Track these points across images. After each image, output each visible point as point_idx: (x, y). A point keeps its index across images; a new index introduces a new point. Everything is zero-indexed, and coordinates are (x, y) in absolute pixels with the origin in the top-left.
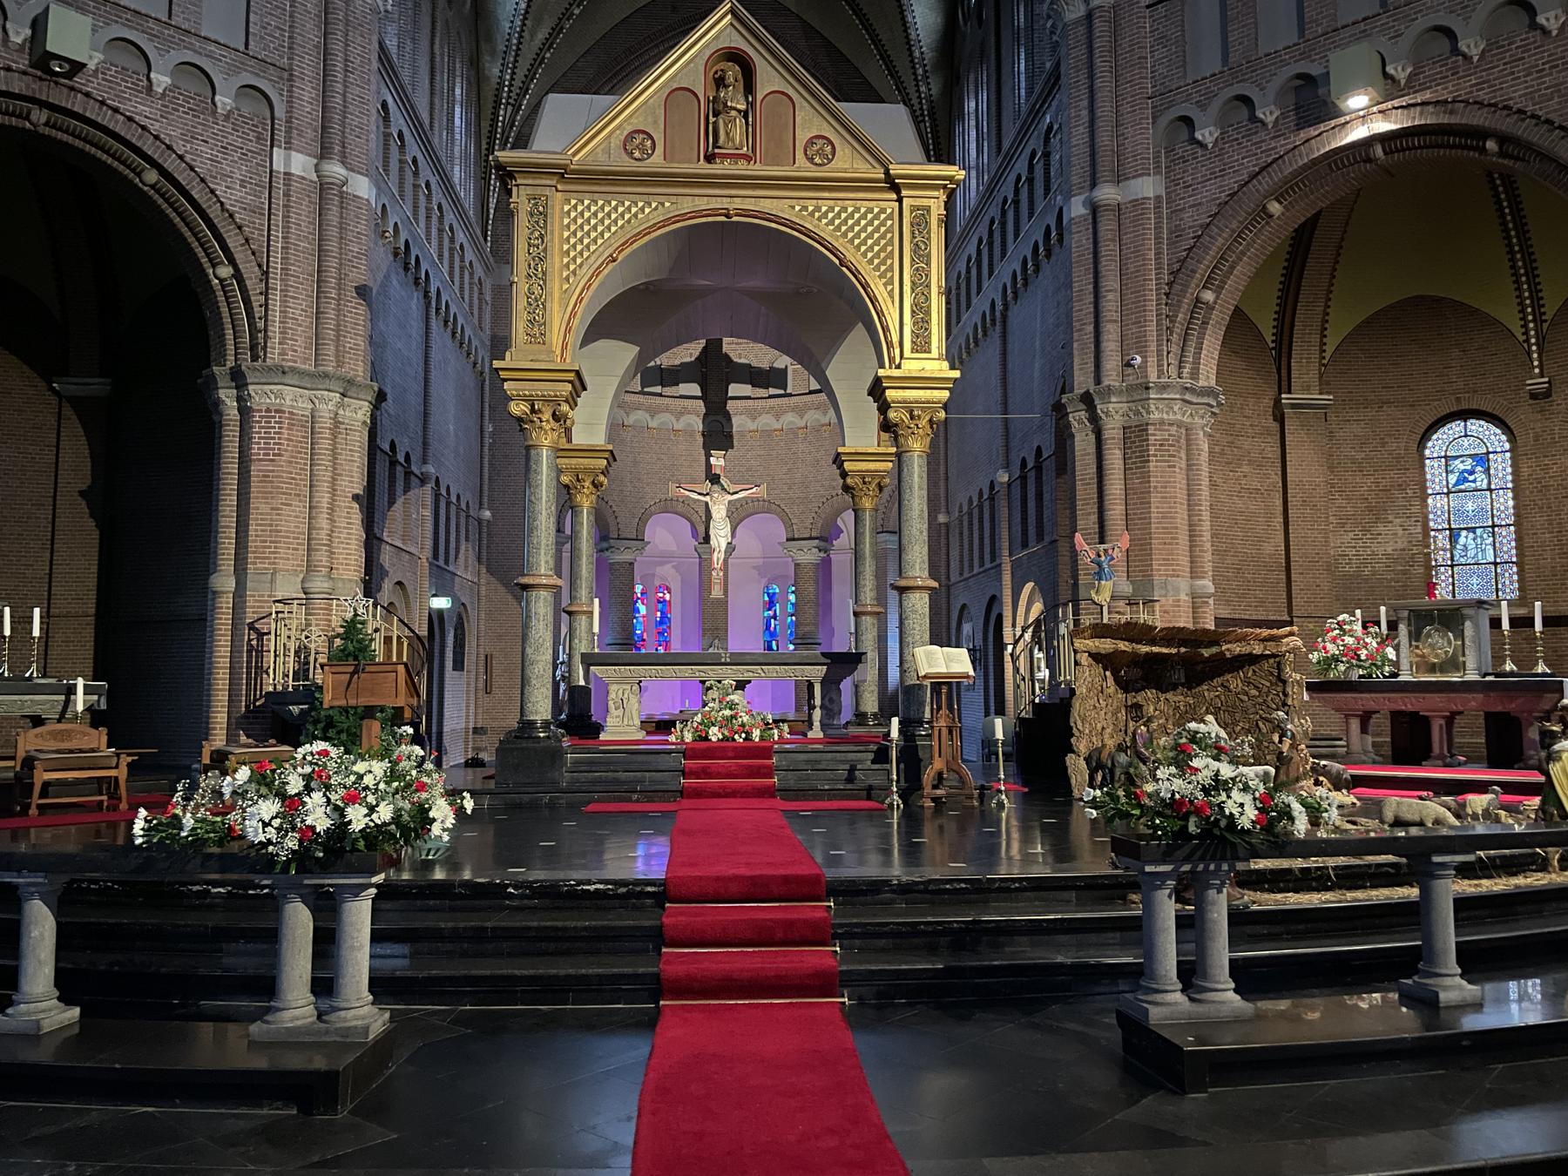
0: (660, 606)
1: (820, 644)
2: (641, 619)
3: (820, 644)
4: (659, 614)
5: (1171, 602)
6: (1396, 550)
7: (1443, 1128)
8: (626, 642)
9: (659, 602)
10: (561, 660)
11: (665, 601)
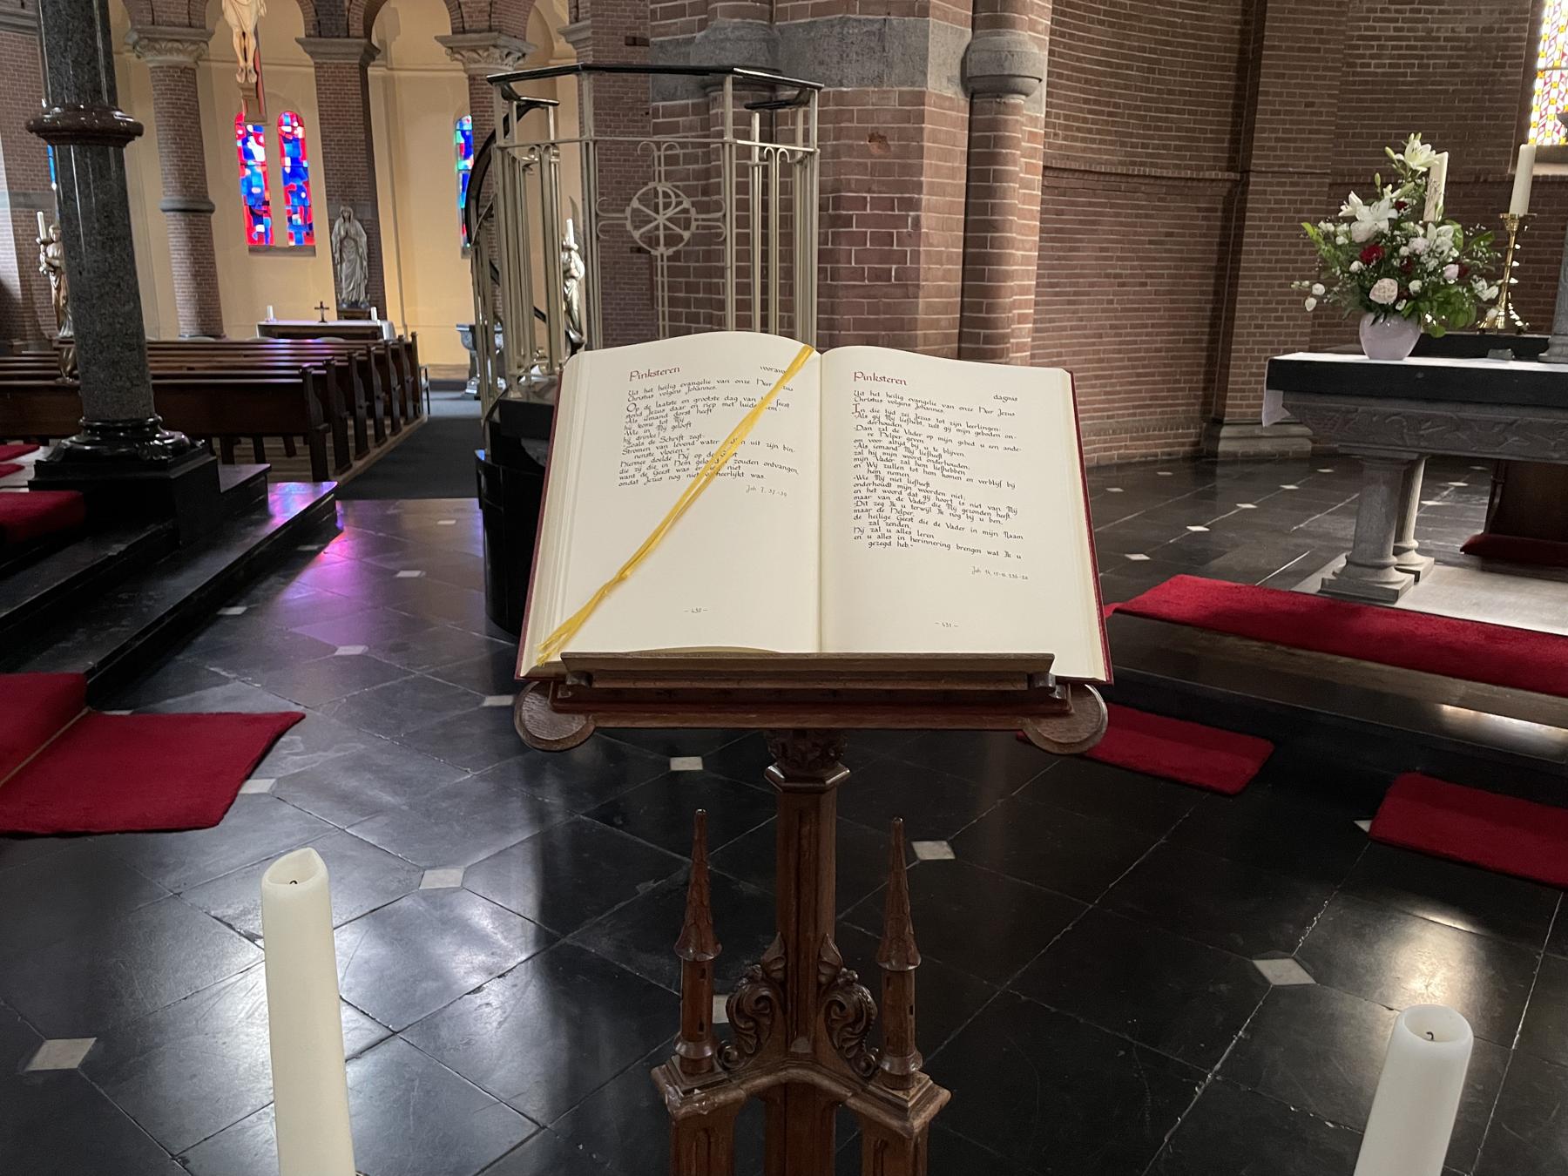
0: (287, 147)
1: (164, 211)
2: (259, 170)
3: (164, 211)
4: (288, 161)
5: (894, 104)
6: (1475, 30)
7: (169, 701)
8: (192, 206)
9: (286, 141)
10: (43, 236)
11: (296, 140)
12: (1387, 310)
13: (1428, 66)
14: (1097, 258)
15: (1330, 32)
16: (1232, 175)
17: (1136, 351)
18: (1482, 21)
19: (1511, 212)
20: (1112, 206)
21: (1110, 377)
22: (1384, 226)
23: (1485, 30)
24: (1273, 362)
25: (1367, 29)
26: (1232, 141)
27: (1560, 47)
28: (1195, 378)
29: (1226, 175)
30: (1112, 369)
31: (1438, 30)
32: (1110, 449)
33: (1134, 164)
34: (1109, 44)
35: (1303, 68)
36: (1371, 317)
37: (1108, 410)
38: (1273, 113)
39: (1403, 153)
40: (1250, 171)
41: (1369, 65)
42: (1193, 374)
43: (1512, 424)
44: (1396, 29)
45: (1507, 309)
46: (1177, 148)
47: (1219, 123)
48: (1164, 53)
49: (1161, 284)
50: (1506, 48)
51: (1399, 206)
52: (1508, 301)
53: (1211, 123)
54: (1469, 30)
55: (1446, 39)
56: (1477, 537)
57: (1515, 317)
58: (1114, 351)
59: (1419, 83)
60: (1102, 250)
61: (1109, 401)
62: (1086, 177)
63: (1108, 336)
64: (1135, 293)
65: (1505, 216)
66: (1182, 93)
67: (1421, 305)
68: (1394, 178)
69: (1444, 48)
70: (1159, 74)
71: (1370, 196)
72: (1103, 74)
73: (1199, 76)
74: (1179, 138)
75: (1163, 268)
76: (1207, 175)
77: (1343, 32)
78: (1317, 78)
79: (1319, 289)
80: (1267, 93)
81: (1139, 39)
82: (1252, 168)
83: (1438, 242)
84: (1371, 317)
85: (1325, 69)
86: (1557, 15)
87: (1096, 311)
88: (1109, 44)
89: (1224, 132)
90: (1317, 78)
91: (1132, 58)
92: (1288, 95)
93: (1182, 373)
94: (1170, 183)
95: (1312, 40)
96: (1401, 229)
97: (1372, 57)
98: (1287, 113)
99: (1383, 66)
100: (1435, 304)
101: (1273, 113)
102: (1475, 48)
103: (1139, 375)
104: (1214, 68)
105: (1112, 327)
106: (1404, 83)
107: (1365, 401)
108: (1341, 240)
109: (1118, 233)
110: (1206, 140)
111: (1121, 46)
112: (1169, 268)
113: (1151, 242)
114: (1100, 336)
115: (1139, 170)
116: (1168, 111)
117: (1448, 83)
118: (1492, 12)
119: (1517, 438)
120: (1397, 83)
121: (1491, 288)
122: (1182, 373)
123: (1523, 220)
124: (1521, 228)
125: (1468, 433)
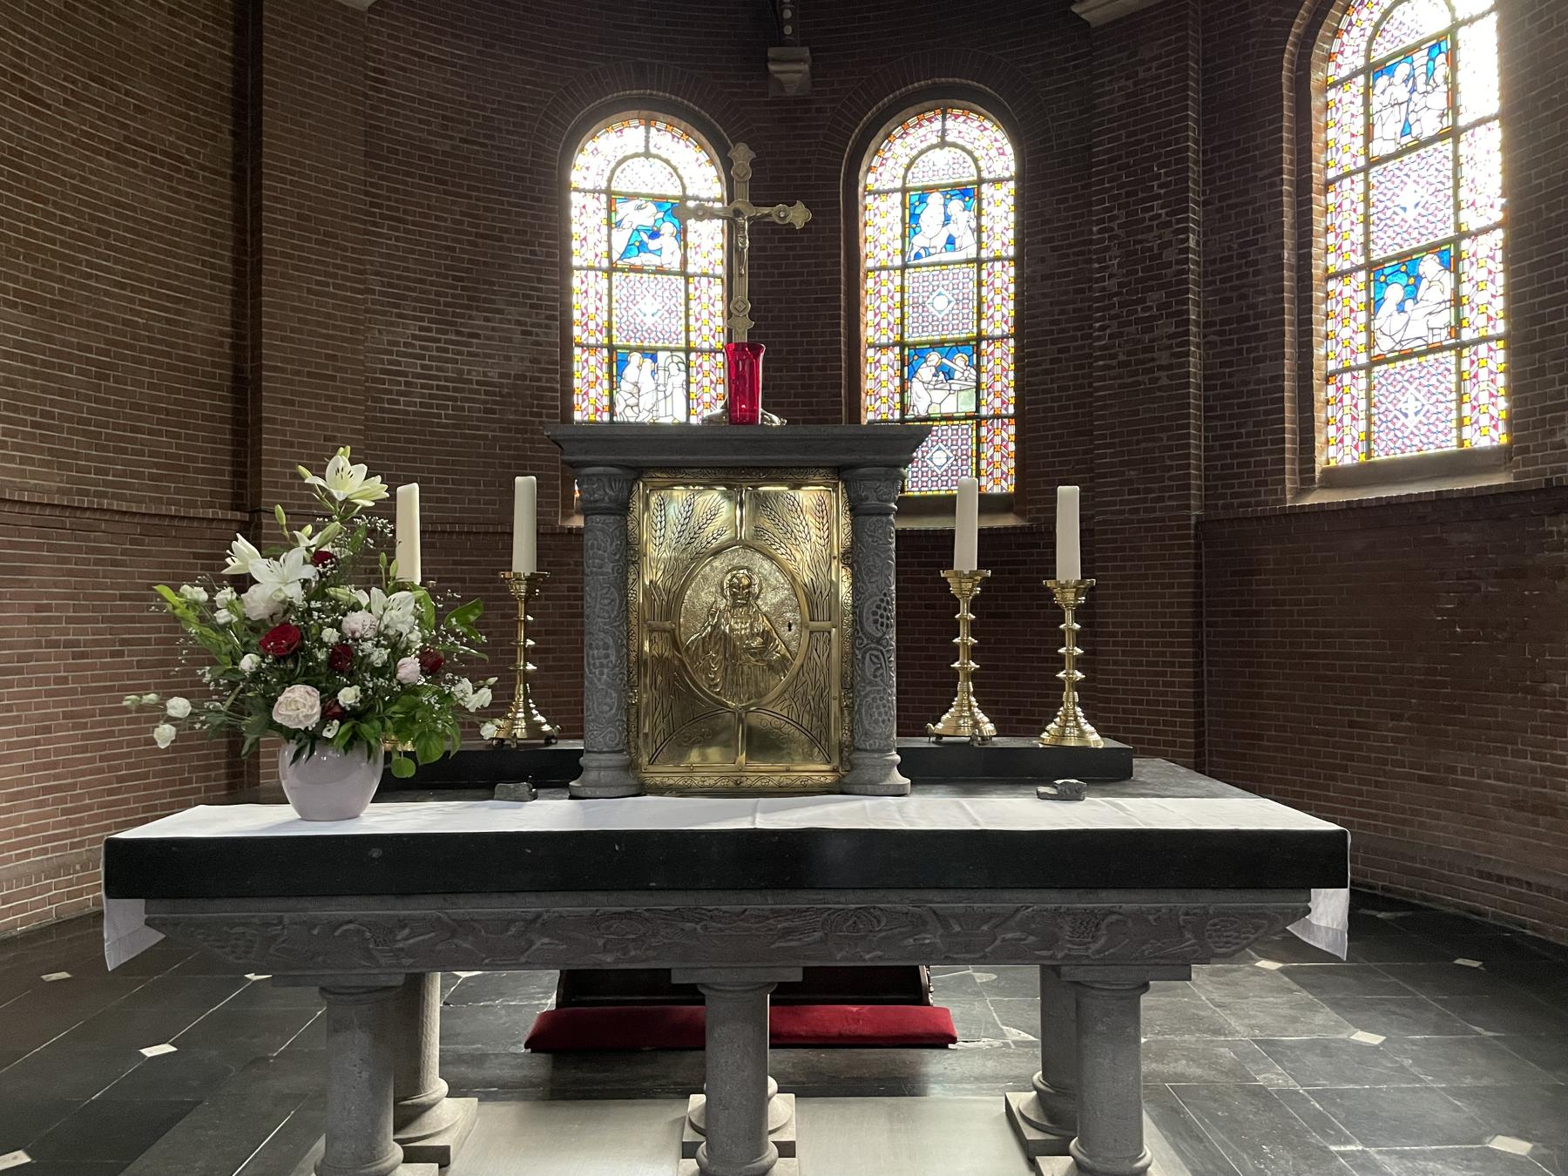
6: (508, 376)
12: (309, 740)
13: (463, 409)
14: (30, 620)
15: (345, 360)
16: (238, 515)
17: (112, 745)
18: (515, 367)
19: (516, 568)
20: (51, 548)
21: (73, 786)
22: (295, 593)
23: (517, 377)
24: (113, 846)
25: (391, 363)
26: (234, 474)
27: (592, 401)
28: (213, 773)
29: (230, 514)
30: (74, 775)
31: (469, 372)
32: (80, 893)
33: (81, 493)
34: (26, 333)
35: (317, 396)
36: (292, 747)
37: (72, 835)
38: (284, 444)
39: (324, 478)
40: (261, 510)
41: (397, 402)
42: (208, 768)
43: (534, 920)
44: (423, 367)
45: (527, 710)
46: (152, 477)
47: (215, 451)
48: (119, 356)
49: (147, 653)
50: (540, 398)
51: (319, 558)
52: (527, 696)
53: (200, 450)
54: (501, 376)
55: (478, 383)
56: (546, 1016)
57: (540, 718)
58: (76, 750)
59: (455, 426)
60: (39, 608)
61: (71, 823)
62: (27, 510)
63: (60, 728)
64: (104, 666)
65: (507, 575)
66: (153, 410)
67: (365, 727)
68: (312, 509)
69: (477, 392)
70: (115, 382)
71: (271, 545)
72: (22, 372)
73: (178, 391)
74: (157, 466)
75: (150, 630)
76: (201, 513)
77: (362, 363)
78: (335, 409)
79: (179, 706)
80: (272, 421)
81: (78, 334)
82: (263, 507)
83: (386, 619)
84: (292, 747)
85: (344, 400)
86: (586, 371)
87: (37, 694)
88: (26, 333)
89: (223, 462)
90: (335, 409)
91: (71, 357)
92: (301, 425)
93: (192, 770)
94: (146, 521)
95: (326, 367)
96: (325, 597)
97: (400, 393)
98: (302, 445)
99: (415, 404)
100: (389, 723)
101: (284, 444)
102: (509, 395)
103: (121, 779)
104: (200, 384)
105: (66, 716)
106: (439, 425)
107: (292, 902)
108: (222, 616)
109: (66, 585)
110: (197, 470)
111: (49, 339)
112: (158, 630)
113: (123, 597)
114: (47, 729)
115: (99, 504)
116: (134, 429)
117: (486, 428)
118: (522, 359)
119: (546, 940)
120: (431, 424)
121: (482, 691)
122: (192, 770)
123: (532, 581)
124: (530, 591)
125: (470, 938)
